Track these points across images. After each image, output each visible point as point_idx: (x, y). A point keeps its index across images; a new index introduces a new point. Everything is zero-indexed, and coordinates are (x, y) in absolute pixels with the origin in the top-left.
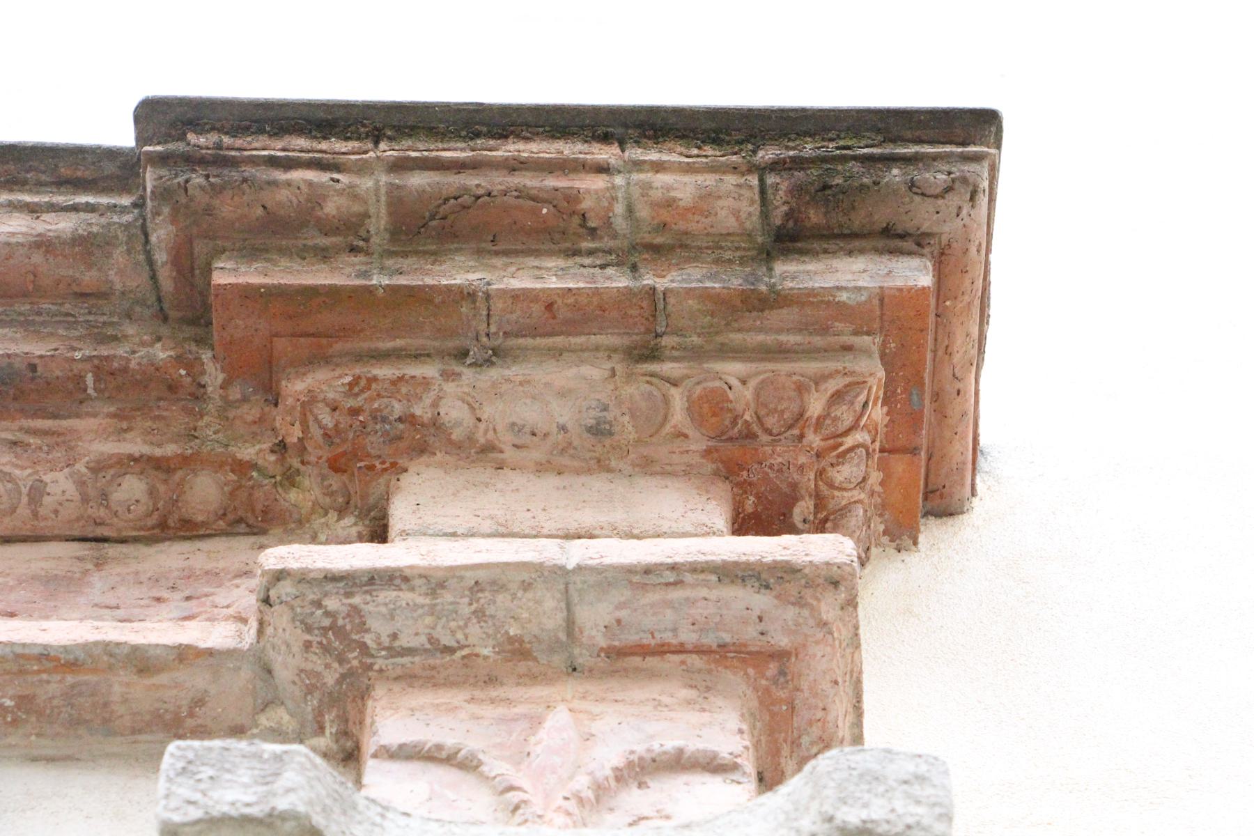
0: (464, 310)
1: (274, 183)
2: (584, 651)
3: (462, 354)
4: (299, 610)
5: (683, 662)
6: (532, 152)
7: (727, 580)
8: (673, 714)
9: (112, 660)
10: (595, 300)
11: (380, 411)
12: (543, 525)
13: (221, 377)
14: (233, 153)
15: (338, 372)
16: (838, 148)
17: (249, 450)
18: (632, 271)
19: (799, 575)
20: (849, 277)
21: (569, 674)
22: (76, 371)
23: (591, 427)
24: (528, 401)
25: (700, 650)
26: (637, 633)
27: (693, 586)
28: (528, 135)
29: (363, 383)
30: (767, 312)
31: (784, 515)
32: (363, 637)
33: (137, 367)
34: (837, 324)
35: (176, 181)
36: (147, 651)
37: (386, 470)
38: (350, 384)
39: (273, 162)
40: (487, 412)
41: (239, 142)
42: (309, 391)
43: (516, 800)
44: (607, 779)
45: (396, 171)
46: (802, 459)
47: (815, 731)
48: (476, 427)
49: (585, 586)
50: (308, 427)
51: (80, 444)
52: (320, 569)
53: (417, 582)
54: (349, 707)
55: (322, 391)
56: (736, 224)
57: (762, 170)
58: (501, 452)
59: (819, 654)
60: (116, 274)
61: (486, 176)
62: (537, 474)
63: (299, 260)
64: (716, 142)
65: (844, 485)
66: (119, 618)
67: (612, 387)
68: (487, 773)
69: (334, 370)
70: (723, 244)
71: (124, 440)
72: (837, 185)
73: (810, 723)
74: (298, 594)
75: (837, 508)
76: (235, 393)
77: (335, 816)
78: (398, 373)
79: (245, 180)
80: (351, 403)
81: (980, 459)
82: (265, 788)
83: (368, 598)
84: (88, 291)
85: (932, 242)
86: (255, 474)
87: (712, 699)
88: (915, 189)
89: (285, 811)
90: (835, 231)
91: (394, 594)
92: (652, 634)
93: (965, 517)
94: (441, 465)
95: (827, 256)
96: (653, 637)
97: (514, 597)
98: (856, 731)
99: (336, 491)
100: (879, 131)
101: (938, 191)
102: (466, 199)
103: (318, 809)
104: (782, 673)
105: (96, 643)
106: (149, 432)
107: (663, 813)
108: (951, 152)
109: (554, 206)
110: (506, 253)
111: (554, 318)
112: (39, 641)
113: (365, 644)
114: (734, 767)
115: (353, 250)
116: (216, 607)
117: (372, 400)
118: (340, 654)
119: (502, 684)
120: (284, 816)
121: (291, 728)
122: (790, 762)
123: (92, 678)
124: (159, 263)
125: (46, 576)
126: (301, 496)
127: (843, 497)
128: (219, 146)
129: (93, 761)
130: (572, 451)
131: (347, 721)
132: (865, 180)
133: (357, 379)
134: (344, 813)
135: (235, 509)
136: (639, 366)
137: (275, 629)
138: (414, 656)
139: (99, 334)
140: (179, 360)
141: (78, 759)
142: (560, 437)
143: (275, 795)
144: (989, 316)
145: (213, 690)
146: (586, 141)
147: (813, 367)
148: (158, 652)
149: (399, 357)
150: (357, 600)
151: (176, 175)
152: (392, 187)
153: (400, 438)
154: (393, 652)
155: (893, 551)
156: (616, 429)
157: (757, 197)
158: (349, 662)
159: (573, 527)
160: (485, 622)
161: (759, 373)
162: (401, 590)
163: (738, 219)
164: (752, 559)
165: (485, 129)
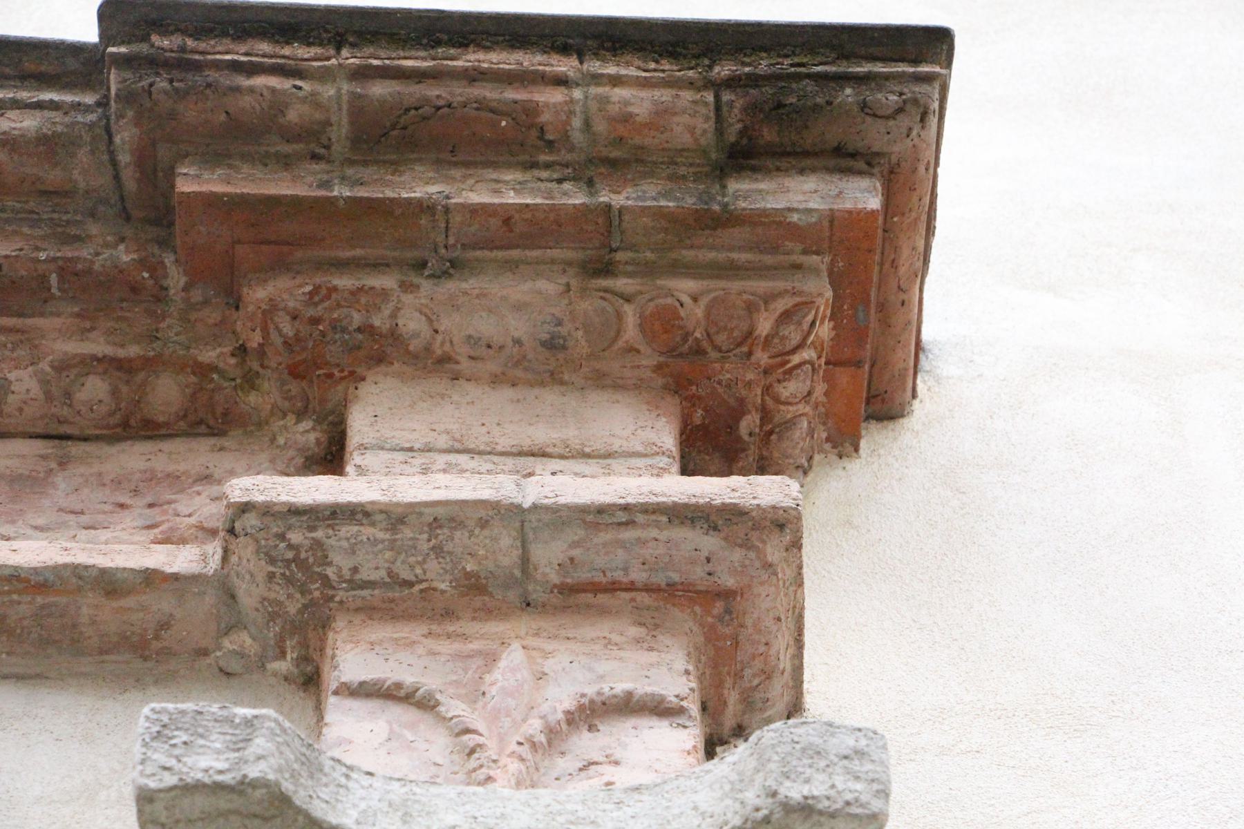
0: (423, 222)
1: (237, 89)
2: (538, 588)
3: (421, 265)
4: (263, 542)
5: (633, 600)
6: (492, 63)
7: (676, 521)
8: (622, 654)
9: (81, 583)
10: (552, 216)
11: (340, 321)
12: (497, 440)
13: (183, 280)
14: (197, 57)
15: (299, 280)
16: (792, 65)
17: (210, 353)
18: (588, 187)
19: (745, 518)
20: (801, 198)
21: (523, 610)
22: (40, 272)
23: (546, 341)
24: (484, 314)
25: (649, 589)
26: (589, 571)
27: (645, 526)
28: (488, 44)
29: (324, 292)
30: (720, 230)
31: (731, 428)
32: (325, 570)
33: (101, 269)
34: (787, 243)
35: (141, 84)
36: (114, 575)
37: (342, 378)
38: (310, 293)
39: (236, 67)
40: (444, 324)
41: (202, 46)
42: (271, 300)
43: (471, 744)
44: (559, 723)
45: (356, 79)
46: (750, 376)
47: (758, 664)
48: (434, 339)
49: (541, 524)
50: (268, 334)
51: (44, 342)
52: (284, 503)
53: (379, 517)
54: (311, 635)
55: (283, 300)
56: (691, 140)
57: (718, 86)
58: (457, 363)
59: (764, 595)
60: (79, 174)
61: (448, 86)
62: (492, 385)
63: (261, 167)
64: (673, 55)
65: (790, 400)
66: (85, 525)
67: (566, 301)
68: (444, 714)
69: (294, 278)
70: (679, 160)
71: (87, 339)
72: (791, 104)
73: (753, 657)
74: (262, 526)
75: (782, 421)
76: (197, 295)
77: (302, 780)
78: (358, 284)
79: (209, 85)
80: (311, 312)
81: (922, 356)
82: (236, 755)
83: (331, 532)
84: (51, 189)
85: (882, 162)
86: (215, 376)
87: (660, 637)
88: (867, 110)
89: (257, 779)
90: (788, 149)
91: (356, 528)
92: (604, 572)
93: (904, 421)
94: (400, 376)
95: (780, 174)
96: (605, 575)
97: (471, 535)
98: (797, 662)
99: (295, 396)
100: (833, 48)
101: (889, 112)
102: (426, 110)
103: (287, 775)
104: (728, 611)
105: (65, 566)
106: (109, 332)
107: (613, 758)
108: (904, 72)
109: (513, 119)
110: (467, 165)
111: (511, 231)
112: (11, 562)
113: (327, 576)
114: (680, 711)
115: (315, 157)
116: (178, 515)
117: (331, 309)
118: (302, 585)
119: (458, 618)
120: (255, 784)
121: (253, 651)
122: (732, 693)
123: (62, 600)
124: (123, 164)
125: (10, 475)
126: (261, 400)
127: (788, 412)
128: (183, 49)
129: (62, 680)
130: (526, 364)
131: (308, 647)
132: (818, 100)
133: (317, 289)
134: (311, 776)
135: (196, 410)
136: (593, 281)
137: (240, 558)
138: (374, 589)
139: (63, 233)
140: (142, 263)
141: (47, 678)
142: (515, 350)
143: (246, 762)
144: (935, 227)
145: (178, 613)
146: (545, 52)
147: (762, 286)
148: (126, 575)
149: (358, 266)
150: (319, 534)
151: (141, 78)
152: (355, 97)
153: (359, 348)
154: (355, 585)
155: (834, 458)
156: (570, 343)
157: (712, 114)
158: (311, 593)
159: (526, 444)
160: (443, 558)
161: (709, 291)
162: (362, 524)
163: (693, 134)
164: (701, 501)
165: (446, 37)
